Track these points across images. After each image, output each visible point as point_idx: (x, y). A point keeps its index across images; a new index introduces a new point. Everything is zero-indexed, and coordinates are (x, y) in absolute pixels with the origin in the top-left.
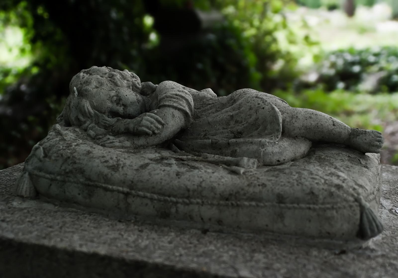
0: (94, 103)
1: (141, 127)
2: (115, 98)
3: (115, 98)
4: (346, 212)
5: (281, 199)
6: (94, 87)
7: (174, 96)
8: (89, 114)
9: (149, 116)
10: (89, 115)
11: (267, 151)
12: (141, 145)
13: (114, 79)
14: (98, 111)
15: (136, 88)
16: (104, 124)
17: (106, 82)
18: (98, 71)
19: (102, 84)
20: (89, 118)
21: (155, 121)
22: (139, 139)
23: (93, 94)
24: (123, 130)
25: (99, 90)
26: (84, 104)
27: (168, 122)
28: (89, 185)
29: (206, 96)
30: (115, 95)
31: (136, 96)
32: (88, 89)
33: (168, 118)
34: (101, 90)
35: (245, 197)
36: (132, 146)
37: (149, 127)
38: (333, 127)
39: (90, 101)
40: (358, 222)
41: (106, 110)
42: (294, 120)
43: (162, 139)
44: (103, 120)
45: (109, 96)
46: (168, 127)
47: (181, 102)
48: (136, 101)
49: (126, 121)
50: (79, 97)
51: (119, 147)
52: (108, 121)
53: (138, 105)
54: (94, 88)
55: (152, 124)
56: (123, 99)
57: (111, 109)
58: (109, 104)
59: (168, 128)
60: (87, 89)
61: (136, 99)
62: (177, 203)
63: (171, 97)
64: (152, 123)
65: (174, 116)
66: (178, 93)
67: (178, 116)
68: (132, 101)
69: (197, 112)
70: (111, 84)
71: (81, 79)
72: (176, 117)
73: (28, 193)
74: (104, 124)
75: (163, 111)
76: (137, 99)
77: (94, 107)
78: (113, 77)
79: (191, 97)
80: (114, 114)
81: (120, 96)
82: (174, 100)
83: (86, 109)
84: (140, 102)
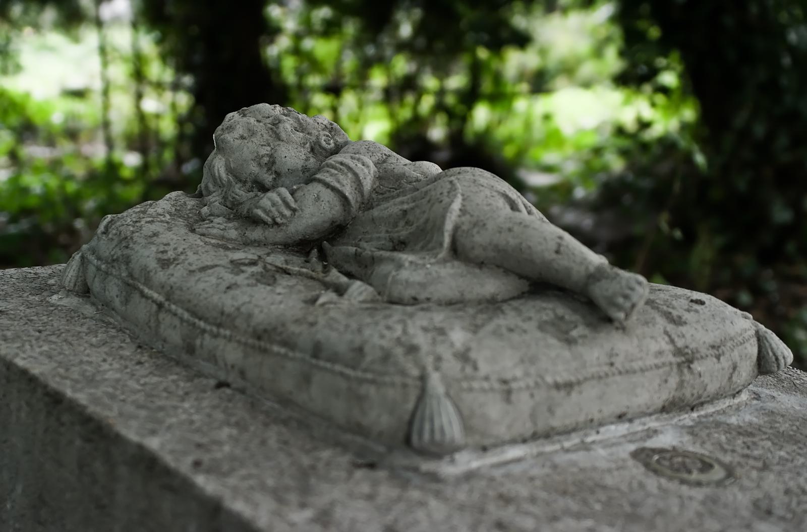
0: (230, 164)
2: (265, 159)
3: (266, 159)
4: (391, 393)
5: (317, 350)
6: (237, 136)
7: (337, 165)
8: (220, 181)
10: (220, 183)
11: (399, 277)
15: (321, 149)
17: (263, 131)
18: (257, 111)
21: (280, 202)
25: (245, 143)
27: (303, 208)
28: (129, 285)
29: (407, 174)
30: (267, 154)
34: (248, 143)
35: (278, 338)
36: (240, 239)
37: (267, 210)
38: (554, 256)
39: (227, 159)
40: (407, 417)
42: (475, 230)
43: (291, 235)
45: (256, 155)
46: (302, 216)
47: (341, 177)
49: (659, 286)
51: (216, 236)
52: (239, 196)
54: (237, 139)
55: (273, 206)
58: (254, 168)
59: (302, 217)
60: (225, 139)
61: (301, 166)
62: (204, 331)
67: (327, 200)
69: (375, 200)
70: (270, 136)
72: (323, 201)
73: (72, 285)
77: (229, 170)
83: (216, 172)
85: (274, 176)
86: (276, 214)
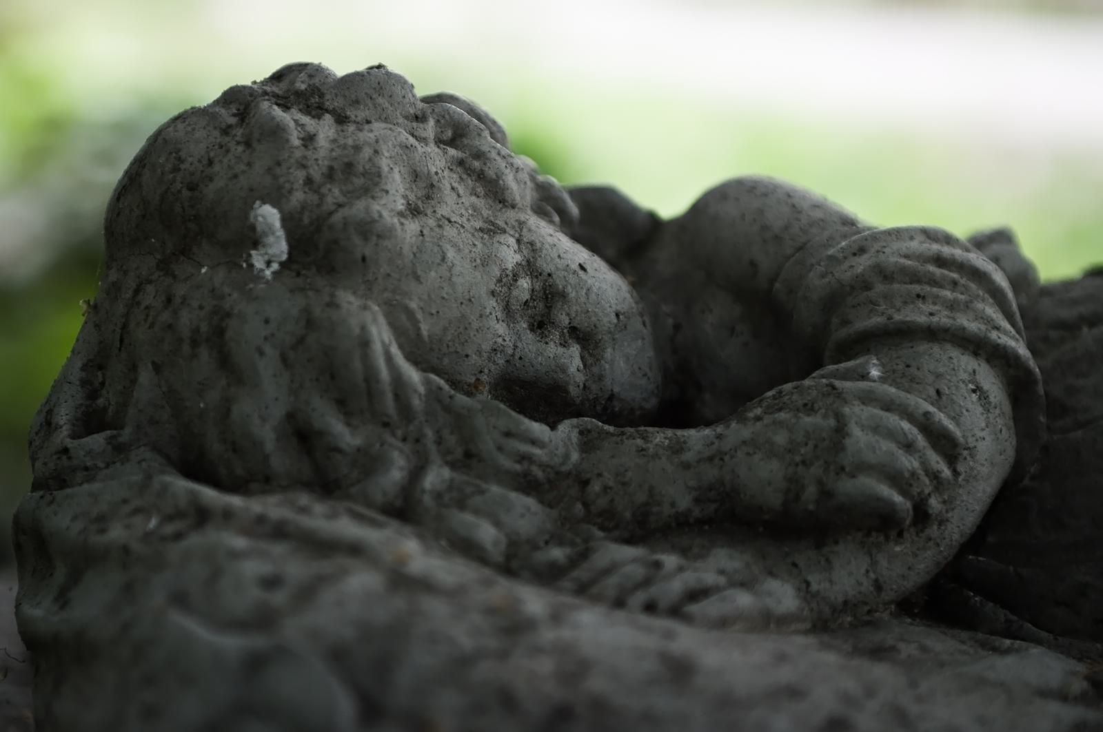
0: (415, 322)
1: (853, 476)
8: (397, 397)
12: (845, 603)
16: (518, 467)
19: (432, 186)
20: (386, 425)
21: (915, 431)
22: (828, 561)
23: (400, 254)
24: (684, 502)
26: (363, 328)
32: (376, 216)
33: (964, 411)
37: (907, 475)
41: (486, 371)
44: (508, 434)
50: (298, 274)
56: (569, 289)
64: (909, 447)
71: (297, 148)
74: (518, 467)
81: (549, 275)
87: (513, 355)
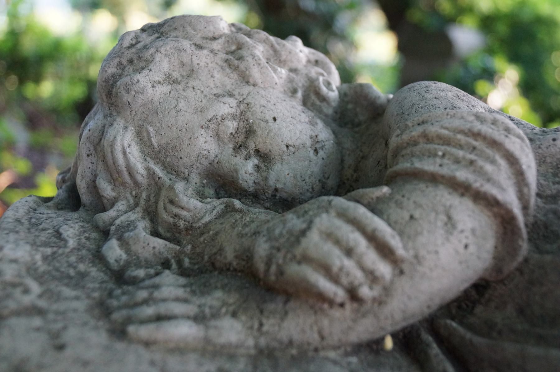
1: (299, 263)
3: (231, 126)
7: (459, 136)
8: (130, 174)
9: (342, 215)
13: (241, 58)
14: (165, 166)
16: (171, 220)
19: (193, 70)
31: (312, 123)
47: (489, 168)
48: (309, 143)
53: (315, 158)
54: (159, 83)
57: (210, 164)
61: (308, 137)
63: (446, 141)
65: (454, 226)
66: (478, 126)
68: (290, 143)
72: (462, 231)
74: (171, 220)
75: (407, 195)
76: (314, 135)
78: (239, 51)
79: (527, 146)
80: (222, 183)
82: (461, 153)
84: (322, 148)
85: (256, 161)
86: (358, 275)
87: (213, 161)
